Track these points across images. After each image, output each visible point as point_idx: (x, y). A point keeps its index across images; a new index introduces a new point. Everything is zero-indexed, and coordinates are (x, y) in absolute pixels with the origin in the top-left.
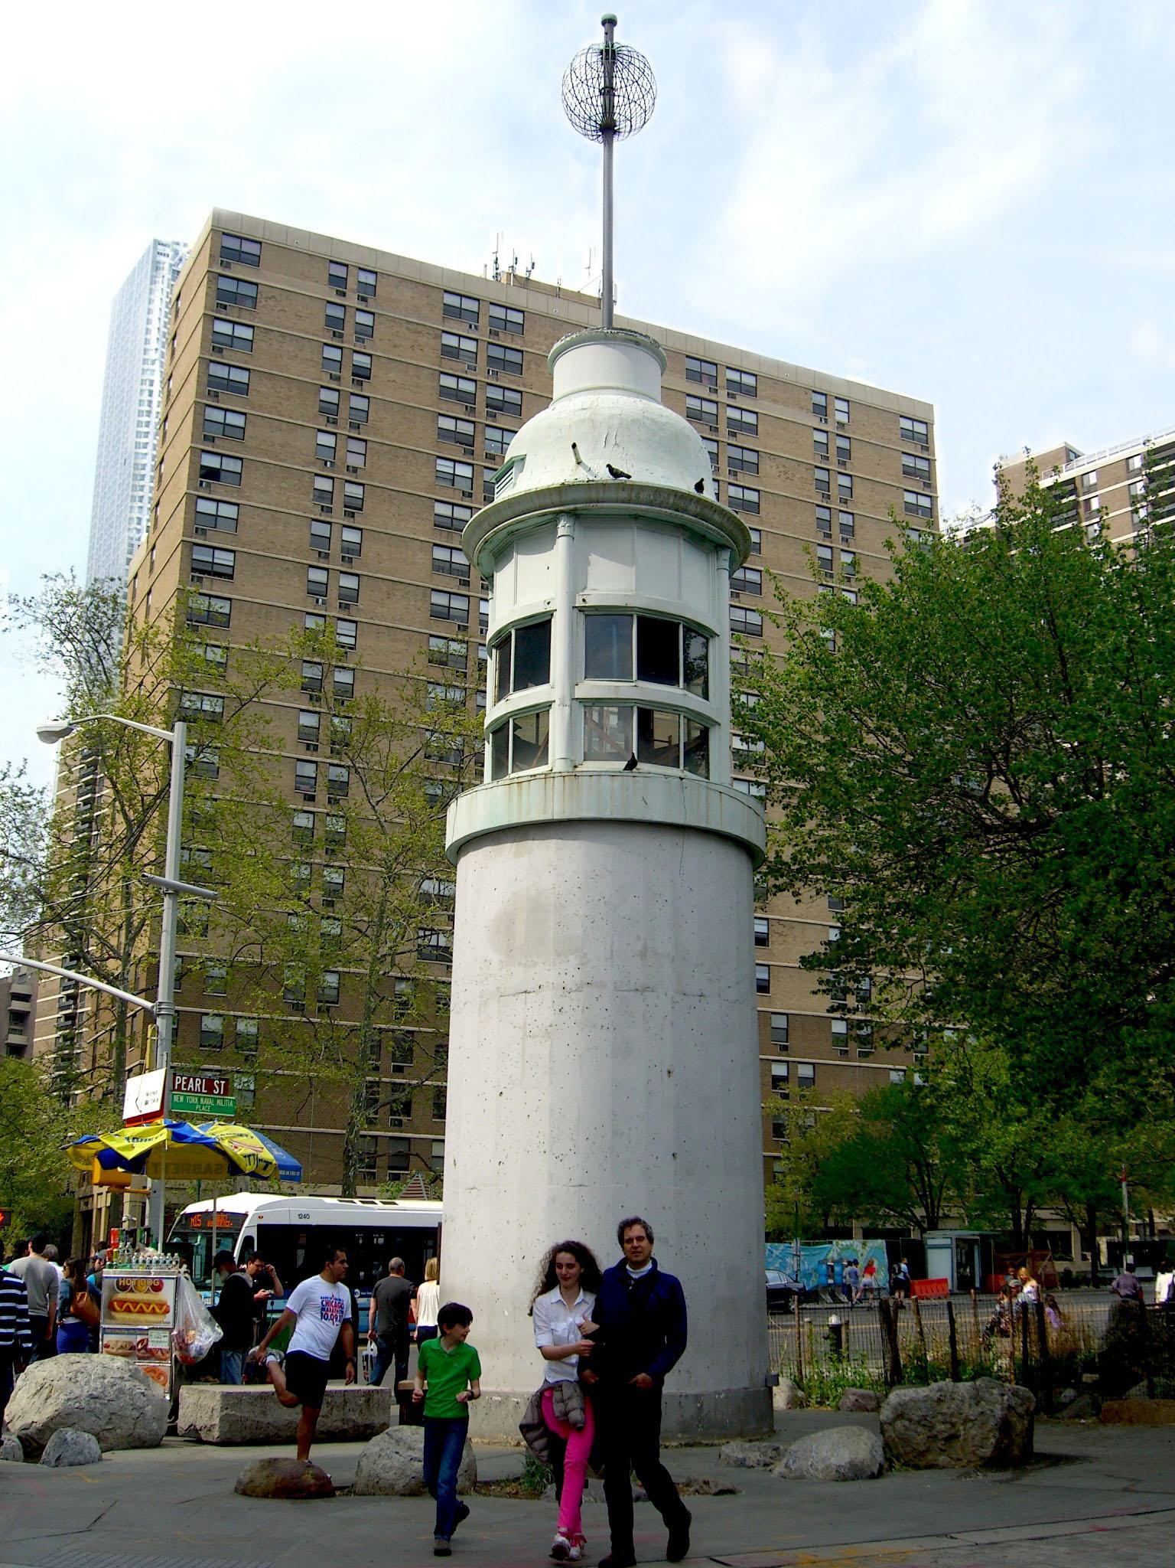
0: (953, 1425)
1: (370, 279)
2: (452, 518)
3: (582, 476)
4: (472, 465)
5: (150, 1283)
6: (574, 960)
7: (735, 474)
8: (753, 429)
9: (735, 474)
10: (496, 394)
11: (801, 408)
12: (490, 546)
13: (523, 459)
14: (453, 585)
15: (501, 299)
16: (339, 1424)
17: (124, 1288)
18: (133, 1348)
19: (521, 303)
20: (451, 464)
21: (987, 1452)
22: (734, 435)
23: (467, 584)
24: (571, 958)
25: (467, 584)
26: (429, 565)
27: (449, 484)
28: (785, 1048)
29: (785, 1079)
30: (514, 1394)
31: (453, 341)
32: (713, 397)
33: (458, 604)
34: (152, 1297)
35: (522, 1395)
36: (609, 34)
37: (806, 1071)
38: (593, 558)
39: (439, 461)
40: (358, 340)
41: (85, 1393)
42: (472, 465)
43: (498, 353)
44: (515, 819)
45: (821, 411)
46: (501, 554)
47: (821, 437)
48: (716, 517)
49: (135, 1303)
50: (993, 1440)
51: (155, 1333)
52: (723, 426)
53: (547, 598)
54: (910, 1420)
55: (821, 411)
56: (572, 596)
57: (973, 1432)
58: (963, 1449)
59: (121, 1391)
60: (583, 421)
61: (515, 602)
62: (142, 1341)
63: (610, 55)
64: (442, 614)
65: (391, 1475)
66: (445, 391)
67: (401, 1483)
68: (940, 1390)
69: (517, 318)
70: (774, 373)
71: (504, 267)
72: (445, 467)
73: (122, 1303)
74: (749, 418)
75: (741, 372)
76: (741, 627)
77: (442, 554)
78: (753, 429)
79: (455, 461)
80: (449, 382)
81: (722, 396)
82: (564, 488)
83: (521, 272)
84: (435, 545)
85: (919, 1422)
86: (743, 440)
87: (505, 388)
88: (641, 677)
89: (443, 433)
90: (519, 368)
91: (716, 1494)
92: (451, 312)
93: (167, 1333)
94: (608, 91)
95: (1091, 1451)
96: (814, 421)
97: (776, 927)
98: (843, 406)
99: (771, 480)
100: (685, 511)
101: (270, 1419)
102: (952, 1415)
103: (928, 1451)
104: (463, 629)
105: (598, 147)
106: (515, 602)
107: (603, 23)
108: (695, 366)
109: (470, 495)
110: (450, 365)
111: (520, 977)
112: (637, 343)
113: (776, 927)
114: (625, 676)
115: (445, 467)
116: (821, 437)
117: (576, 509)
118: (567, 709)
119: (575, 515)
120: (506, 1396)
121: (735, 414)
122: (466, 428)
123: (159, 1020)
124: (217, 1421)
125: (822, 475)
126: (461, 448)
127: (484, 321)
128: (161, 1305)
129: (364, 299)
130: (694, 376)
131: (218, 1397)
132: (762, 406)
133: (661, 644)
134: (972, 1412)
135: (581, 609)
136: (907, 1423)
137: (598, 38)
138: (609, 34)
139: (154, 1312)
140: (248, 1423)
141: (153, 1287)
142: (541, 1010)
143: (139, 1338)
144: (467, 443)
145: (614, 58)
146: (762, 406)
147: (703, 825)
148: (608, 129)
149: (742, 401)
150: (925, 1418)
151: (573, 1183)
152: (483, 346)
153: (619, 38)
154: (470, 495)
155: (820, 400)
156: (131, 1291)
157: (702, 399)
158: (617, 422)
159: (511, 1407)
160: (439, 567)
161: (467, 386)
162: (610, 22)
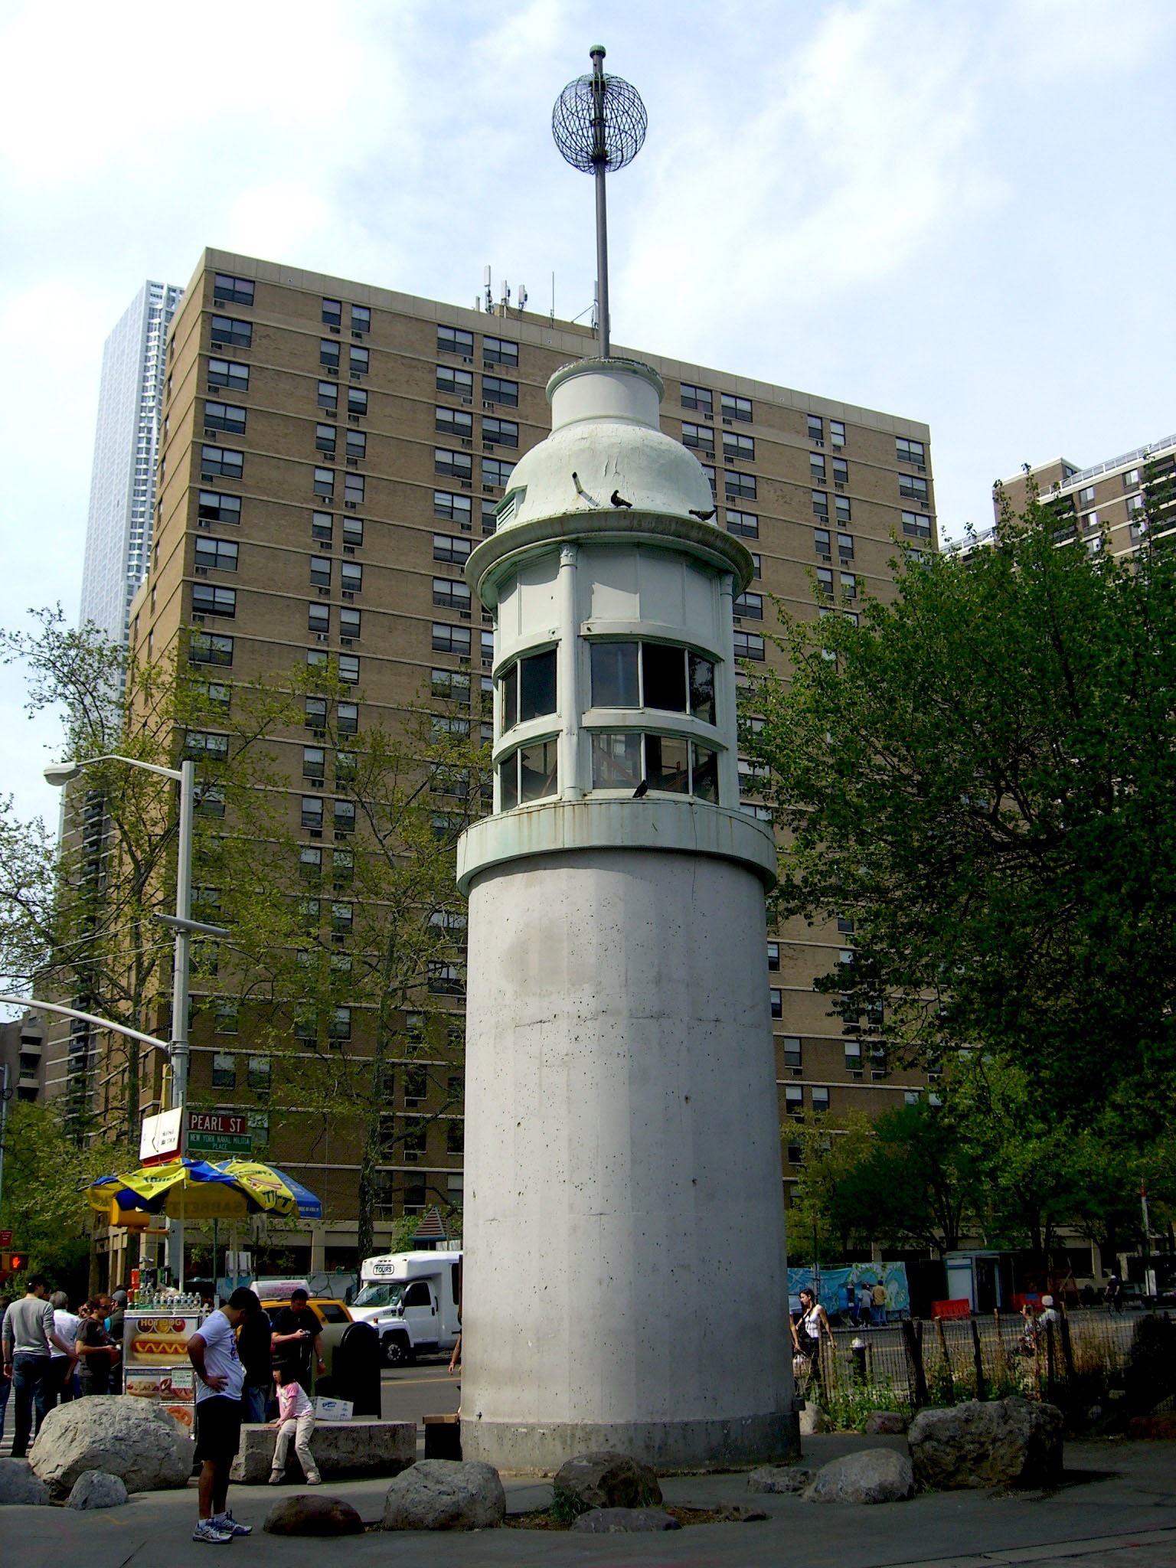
0: (982, 1444)
1: (364, 315)
2: (452, 551)
3: (584, 505)
7: (733, 500)
8: (750, 454)
9: (733, 500)
10: (493, 426)
12: (493, 578)
13: (524, 490)
15: (495, 331)
18: (156, 1388)
19: (514, 335)
20: (449, 497)
21: (1017, 1470)
22: (731, 460)
23: (468, 616)
24: (586, 986)
25: (468, 616)
26: (430, 597)
28: (798, 1072)
29: (799, 1103)
30: (541, 1426)
31: (447, 375)
32: (709, 423)
33: (460, 636)
35: (547, 1426)
36: (598, 66)
37: (820, 1095)
38: (596, 586)
39: (437, 495)
40: (353, 375)
41: (110, 1435)
45: (817, 434)
46: (505, 586)
47: (818, 461)
48: (719, 543)
49: (158, 1344)
50: (1022, 1459)
51: (178, 1373)
52: (720, 454)
53: (551, 627)
54: (938, 1441)
55: (817, 434)
57: (1002, 1451)
59: (146, 1432)
60: (582, 451)
61: (520, 633)
62: (165, 1382)
63: (600, 86)
64: (443, 647)
65: (420, 1510)
66: (441, 425)
67: (430, 1517)
68: (968, 1409)
69: (511, 350)
70: (769, 398)
71: (497, 300)
72: (443, 500)
73: (144, 1343)
74: (746, 444)
75: (736, 397)
77: (442, 587)
78: (750, 454)
79: (453, 494)
80: (445, 416)
81: (718, 422)
82: (565, 518)
83: (514, 304)
84: (436, 578)
85: (947, 1443)
86: (741, 465)
89: (441, 467)
90: (514, 400)
91: (747, 1520)
92: (445, 345)
94: (599, 123)
95: (1120, 1467)
96: (810, 445)
97: (786, 951)
99: (768, 504)
100: (687, 537)
102: (980, 1435)
103: (957, 1471)
104: (465, 661)
105: (590, 180)
106: (520, 633)
107: (592, 55)
108: (689, 393)
109: (469, 528)
110: (446, 399)
112: (635, 372)
113: (786, 951)
114: (632, 703)
115: (443, 500)
116: (818, 461)
117: (578, 539)
118: (575, 738)
119: (577, 545)
120: (532, 1428)
121: (731, 440)
122: (463, 461)
123: (174, 1060)
125: (819, 498)
126: (458, 481)
127: (478, 354)
129: (358, 336)
132: (757, 430)
133: (668, 670)
135: (586, 638)
136: (935, 1444)
138: (598, 66)
141: (174, 1326)
142: (557, 1039)
143: (162, 1378)
144: (464, 475)
146: (757, 430)
148: (599, 161)
149: (738, 427)
150: (953, 1438)
151: (593, 1212)
153: (609, 67)
154: (469, 528)
155: (816, 423)
156: (154, 1331)
159: (537, 1438)
160: (440, 600)
162: (599, 54)
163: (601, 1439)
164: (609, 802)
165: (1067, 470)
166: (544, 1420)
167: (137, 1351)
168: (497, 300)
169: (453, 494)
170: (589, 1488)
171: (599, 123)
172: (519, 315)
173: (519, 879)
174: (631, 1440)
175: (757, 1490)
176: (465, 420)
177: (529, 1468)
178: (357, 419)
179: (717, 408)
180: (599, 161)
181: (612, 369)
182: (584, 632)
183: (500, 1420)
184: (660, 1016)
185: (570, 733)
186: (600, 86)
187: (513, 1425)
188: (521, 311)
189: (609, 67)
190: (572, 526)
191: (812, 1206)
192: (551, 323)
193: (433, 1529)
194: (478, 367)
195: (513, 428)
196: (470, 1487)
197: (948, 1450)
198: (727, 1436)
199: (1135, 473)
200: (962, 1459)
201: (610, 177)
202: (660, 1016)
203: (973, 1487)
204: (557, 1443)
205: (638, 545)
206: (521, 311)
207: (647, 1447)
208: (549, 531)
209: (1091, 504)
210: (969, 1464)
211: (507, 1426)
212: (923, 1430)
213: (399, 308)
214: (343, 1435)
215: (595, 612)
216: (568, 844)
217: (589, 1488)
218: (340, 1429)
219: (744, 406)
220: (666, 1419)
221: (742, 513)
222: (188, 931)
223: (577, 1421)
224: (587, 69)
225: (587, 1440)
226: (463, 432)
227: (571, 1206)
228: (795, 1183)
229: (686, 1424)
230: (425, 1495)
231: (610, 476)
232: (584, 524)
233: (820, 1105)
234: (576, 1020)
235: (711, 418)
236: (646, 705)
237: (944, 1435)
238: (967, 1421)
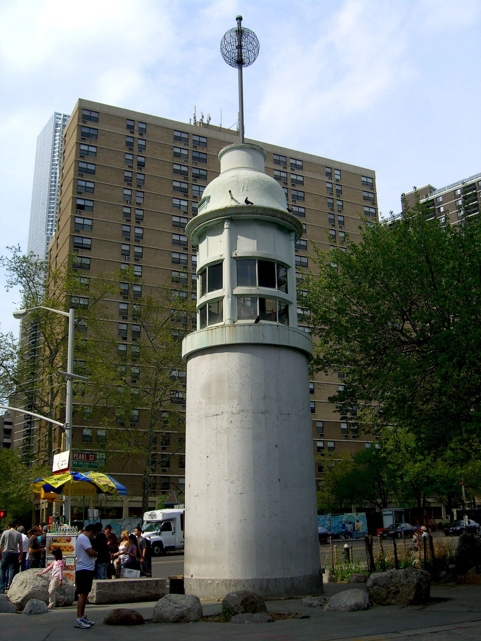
0: (397, 587)
1: (144, 126)
2: (180, 223)
3: (234, 204)
4: (187, 201)
5: (66, 538)
8: (302, 183)
10: (197, 172)
12: (197, 233)
13: (209, 197)
16: (145, 594)
17: (55, 541)
19: (205, 134)
20: (179, 201)
21: (411, 597)
22: (294, 185)
23: (186, 249)
25: (186, 249)
26: (171, 242)
27: (178, 209)
28: (322, 435)
29: (322, 448)
30: (217, 580)
31: (178, 151)
32: (285, 170)
33: (183, 257)
34: (67, 544)
35: (219, 580)
36: (239, 24)
37: (331, 444)
38: (239, 237)
39: (174, 200)
41: (41, 584)
42: (187, 201)
43: (197, 155)
44: (210, 344)
45: (329, 175)
46: (201, 237)
47: (329, 186)
50: (413, 593)
51: (68, 559)
53: (221, 254)
54: (379, 586)
55: (329, 175)
56: (231, 253)
57: (405, 590)
58: (401, 597)
60: (233, 181)
61: (208, 256)
63: (240, 32)
64: (176, 262)
65: (167, 614)
66: (175, 171)
68: (391, 573)
70: (309, 160)
71: (198, 120)
72: (176, 202)
74: (300, 179)
76: (299, 264)
78: (302, 183)
80: (177, 167)
82: (226, 209)
83: (205, 121)
85: (383, 586)
86: (298, 187)
87: (200, 169)
89: (175, 188)
90: (205, 161)
92: (177, 138)
93: (73, 559)
94: (240, 47)
96: (326, 179)
98: (338, 172)
100: (276, 217)
101: (117, 593)
102: (396, 583)
103: (387, 598)
105: (236, 70)
106: (208, 256)
107: (237, 19)
108: (277, 158)
109: (187, 213)
110: (177, 160)
114: (253, 284)
115: (176, 202)
118: (230, 299)
119: (231, 220)
120: (213, 581)
121: (294, 177)
122: (185, 186)
123: (66, 431)
124: (95, 594)
125: (330, 201)
127: (190, 142)
128: (71, 547)
129: (141, 135)
130: (277, 162)
132: (306, 173)
133: (268, 271)
135: (235, 258)
137: (234, 25)
138: (239, 24)
139: (68, 550)
140: (108, 595)
142: (223, 422)
144: (185, 191)
145: (241, 33)
146: (306, 173)
148: (240, 63)
149: (297, 172)
150: (385, 584)
151: (238, 493)
152: (190, 152)
153: (244, 24)
154: (187, 213)
155: (329, 170)
156: (58, 542)
157: (280, 171)
158: (247, 181)
159: (215, 585)
160: (175, 242)
161: (184, 169)
162: (240, 19)
163: (242, 585)
164: (244, 325)
165: (431, 189)
166: (218, 578)
168: (198, 120)
170: (237, 605)
171: (240, 47)
172: (207, 126)
173: (208, 357)
174: (254, 586)
175: (305, 606)
176: (185, 169)
178: (141, 169)
179: (288, 164)
180: (240, 63)
181: (245, 148)
182: (234, 255)
184: (265, 412)
185: (228, 297)
186: (240, 32)
188: (208, 124)
189: (244, 24)
190: (229, 212)
191: (328, 490)
192: (220, 129)
193: (172, 622)
195: (205, 172)
197: (383, 589)
199: (459, 191)
200: (389, 593)
202: (265, 412)
203: (394, 605)
204: (224, 587)
205: (256, 220)
206: (208, 124)
207: (260, 588)
208: (220, 215)
209: (441, 203)
210: (392, 595)
212: (373, 581)
213: (158, 123)
214: (136, 584)
217: (237, 605)
219: (299, 163)
221: (298, 207)
222: (72, 378)
224: (235, 25)
225: (236, 585)
226: (184, 174)
228: (321, 480)
229: (277, 579)
230: (169, 608)
231: (245, 192)
233: (331, 449)
234: (231, 414)
235: (286, 168)
236: (259, 285)
237: (382, 583)
238: (391, 577)
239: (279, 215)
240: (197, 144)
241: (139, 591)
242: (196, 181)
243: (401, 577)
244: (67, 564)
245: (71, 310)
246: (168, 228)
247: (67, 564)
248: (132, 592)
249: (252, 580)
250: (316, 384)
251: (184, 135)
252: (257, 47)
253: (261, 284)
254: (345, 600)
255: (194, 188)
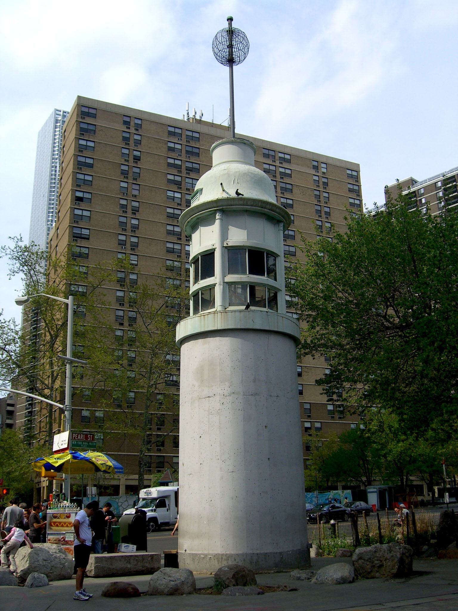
0: (381, 561)
1: (139, 122)
2: (174, 214)
3: (225, 196)
4: (181, 193)
5: (66, 515)
6: (227, 384)
7: (283, 193)
8: (290, 176)
9: (283, 193)
10: (190, 165)
11: (308, 167)
12: (190, 224)
13: (202, 190)
14: (174, 239)
15: (190, 128)
17: (55, 517)
18: (59, 540)
19: (198, 130)
20: (173, 193)
21: (395, 571)
22: (282, 178)
23: (180, 239)
25: (180, 239)
26: (165, 232)
28: (309, 416)
30: (209, 554)
31: (172, 145)
32: (274, 164)
33: (177, 247)
36: (230, 24)
37: (318, 425)
38: (230, 227)
39: (168, 192)
42: (181, 193)
43: (190, 149)
45: (316, 168)
46: (194, 227)
48: (277, 210)
49: (60, 523)
50: (397, 567)
51: (68, 534)
53: (213, 243)
54: (364, 560)
55: (316, 168)
57: (389, 564)
58: (385, 570)
60: (224, 174)
61: (200, 245)
62: (63, 538)
63: (231, 32)
64: (171, 251)
65: (162, 587)
66: (169, 165)
67: (166, 590)
71: (191, 116)
72: (170, 194)
73: (55, 523)
74: (288, 172)
76: (288, 253)
78: (290, 176)
80: (171, 161)
81: (277, 163)
82: (218, 201)
83: (198, 117)
88: (250, 273)
89: (169, 181)
90: (198, 155)
91: (289, 591)
92: (171, 134)
94: (231, 46)
96: (313, 172)
97: (304, 369)
98: (324, 166)
101: (114, 567)
102: (380, 557)
103: (372, 571)
105: (227, 69)
106: (200, 245)
107: (228, 20)
108: (266, 152)
109: (181, 205)
111: (206, 392)
112: (245, 144)
113: (304, 369)
114: (244, 273)
115: (170, 194)
116: (317, 178)
118: (222, 286)
119: (223, 211)
120: (206, 555)
121: (282, 170)
122: (178, 179)
123: (66, 412)
124: (93, 568)
125: (317, 193)
127: (184, 137)
129: (137, 130)
130: (266, 156)
131: (94, 559)
132: (293, 167)
133: (257, 260)
134: (388, 556)
135: (226, 247)
136: (363, 561)
138: (230, 24)
139: (67, 526)
140: (106, 569)
142: (215, 403)
143: (62, 536)
144: (179, 184)
145: (232, 33)
146: (293, 167)
147: (276, 329)
148: (231, 61)
149: (285, 165)
150: (370, 559)
151: (229, 471)
152: (184, 146)
153: (235, 25)
154: (181, 205)
155: (315, 164)
156: (58, 518)
157: (269, 165)
158: (237, 174)
159: (208, 559)
160: (169, 233)
161: (178, 162)
162: (230, 20)
163: (233, 560)
166: (211, 552)
167: (52, 526)
168: (191, 116)
169: (174, 192)
170: (228, 579)
173: (200, 341)
174: (244, 560)
176: (179, 163)
177: (205, 571)
178: (137, 163)
179: (277, 158)
180: (231, 61)
182: (225, 245)
183: (193, 552)
184: (255, 394)
186: (231, 32)
187: (199, 554)
188: (200, 120)
189: (235, 25)
191: (315, 469)
192: (212, 125)
193: (167, 595)
194: (184, 142)
195: (198, 166)
196: (182, 578)
197: (368, 563)
198: (282, 558)
199: (440, 183)
200: (373, 566)
201: (235, 67)
202: (255, 394)
203: (378, 578)
204: (216, 561)
205: (246, 211)
206: (200, 120)
208: (212, 206)
211: (196, 555)
213: (153, 119)
215: (230, 237)
216: (219, 328)
217: (228, 579)
218: (131, 556)
219: (287, 157)
220: (258, 552)
221: (287, 198)
222: (71, 362)
223: (224, 552)
224: (226, 25)
227: (221, 469)
228: (308, 459)
230: (164, 582)
231: (235, 184)
232: (225, 203)
233: (318, 429)
234: (223, 396)
235: (275, 161)
236: (249, 273)
237: (366, 558)
238: (375, 552)
239: (268, 207)
240: (190, 138)
241: (136, 565)
242: (189, 174)
243: (384, 552)
244: (66, 539)
245: (70, 297)
246: (163, 219)
247: (66, 539)
248: (129, 566)
249: (243, 555)
250: (304, 368)
251: (178, 131)
252: (247, 46)
253: (250, 273)
254: (331, 574)
255: (188, 180)
